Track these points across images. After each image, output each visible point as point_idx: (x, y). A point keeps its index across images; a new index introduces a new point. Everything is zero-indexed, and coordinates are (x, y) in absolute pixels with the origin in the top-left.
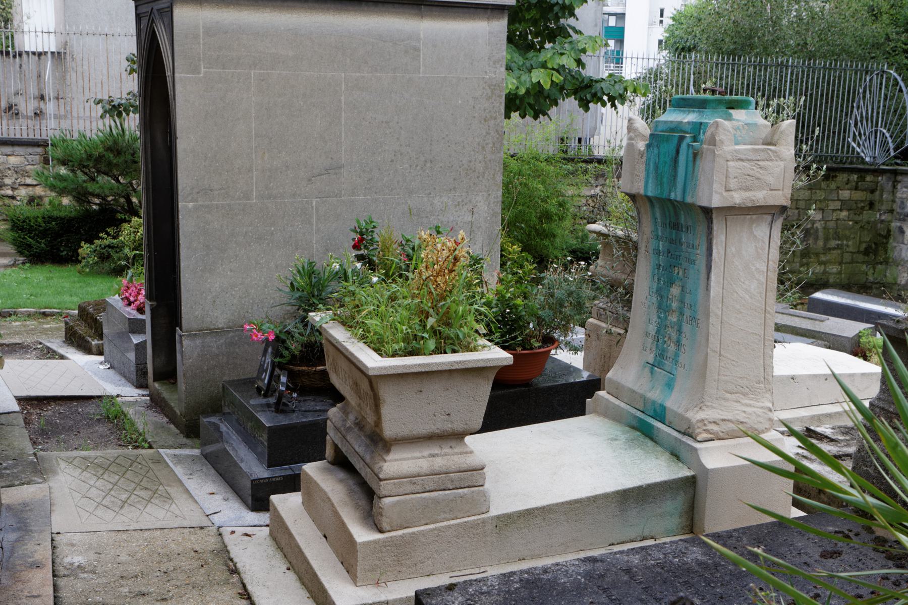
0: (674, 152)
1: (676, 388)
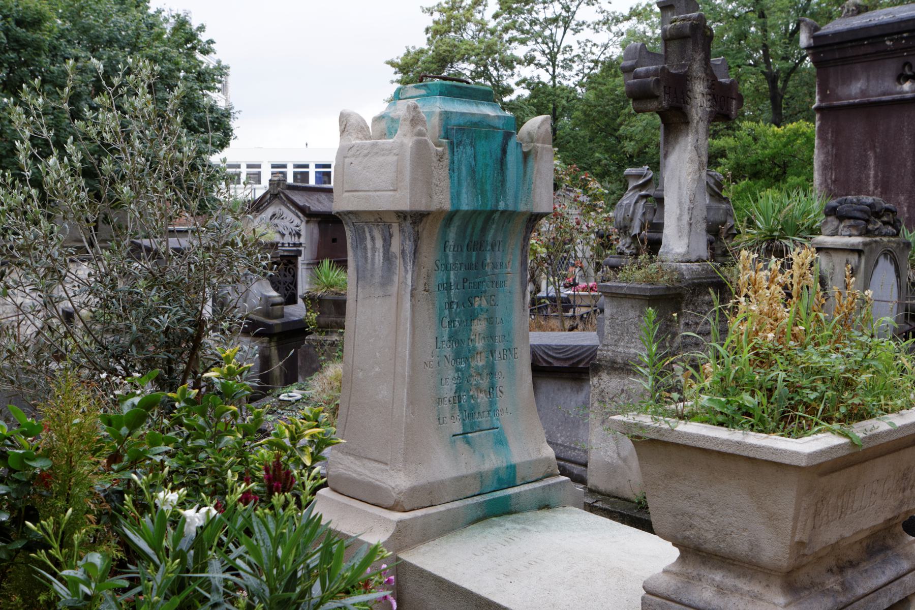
0: (499, 152)
1: (511, 440)
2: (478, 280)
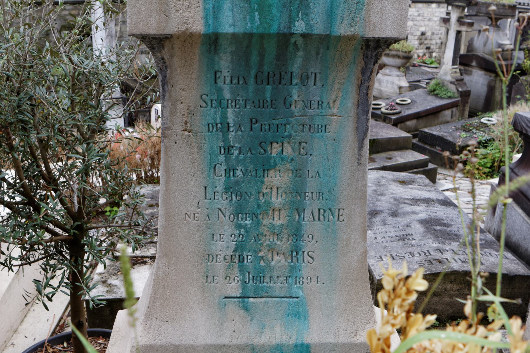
2: (277, 122)
